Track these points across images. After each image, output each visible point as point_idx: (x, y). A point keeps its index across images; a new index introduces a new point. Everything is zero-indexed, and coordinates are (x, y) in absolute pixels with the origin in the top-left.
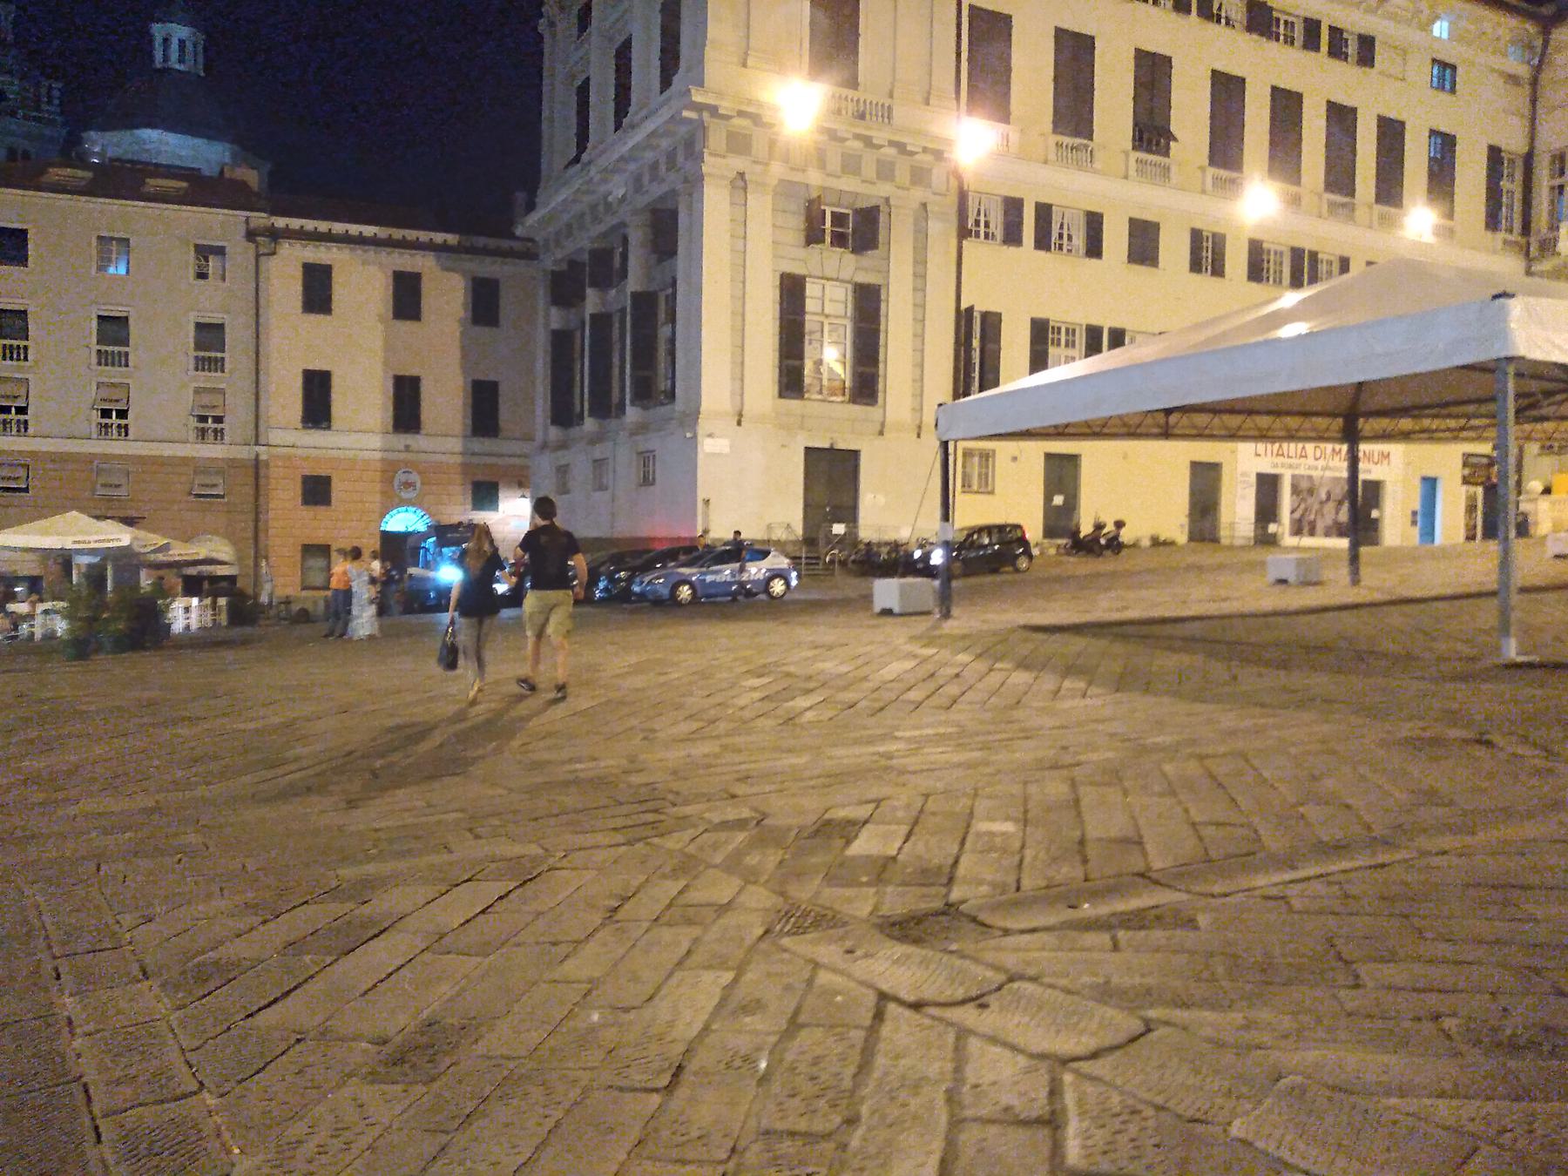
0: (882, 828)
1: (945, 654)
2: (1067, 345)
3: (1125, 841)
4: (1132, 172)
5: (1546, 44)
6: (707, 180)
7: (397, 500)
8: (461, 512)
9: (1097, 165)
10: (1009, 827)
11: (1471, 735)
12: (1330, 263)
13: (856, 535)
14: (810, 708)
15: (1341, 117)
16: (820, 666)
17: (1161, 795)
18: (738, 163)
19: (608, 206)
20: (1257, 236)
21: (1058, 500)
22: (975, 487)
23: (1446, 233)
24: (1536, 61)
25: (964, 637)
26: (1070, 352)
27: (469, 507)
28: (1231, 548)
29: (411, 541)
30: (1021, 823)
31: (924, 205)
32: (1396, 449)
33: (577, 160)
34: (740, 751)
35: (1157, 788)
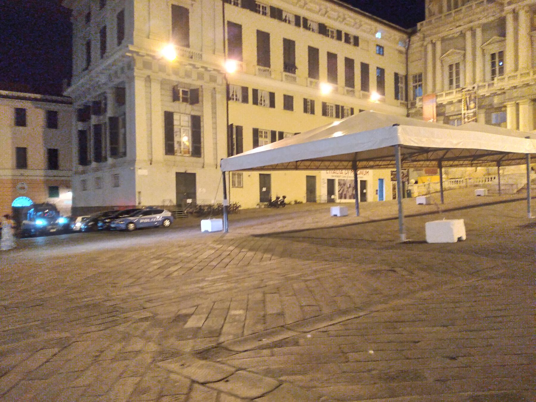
0: (198, 316)
1: (225, 247)
2: (265, 137)
3: (279, 314)
4: (284, 79)
5: (409, 41)
6: (136, 78)
7: (18, 194)
8: (45, 198)
9: (273, 76)
10: (241, 312)
11: (387, 268)
12: (348, 110)
13: (196, 203)
14: (176, 271)
15: (349, 63)
16: (180, 254)
17: (292, 296)
18: (148, 72)
19: (99, 87)
20: (325, 101)
21: (264, 189)
22: (236, 185)
23: (383, 101)
24: (407, 47)
25: (232, 240)
26: (266, 140)
27: (48, 196)
28: (320, 204)
29: (24, 212)
30: (245, 310)
31: (214, 88)
32: (371, 171)
33: (87, 69)
34: (147, 289)
35: (290, 294)
